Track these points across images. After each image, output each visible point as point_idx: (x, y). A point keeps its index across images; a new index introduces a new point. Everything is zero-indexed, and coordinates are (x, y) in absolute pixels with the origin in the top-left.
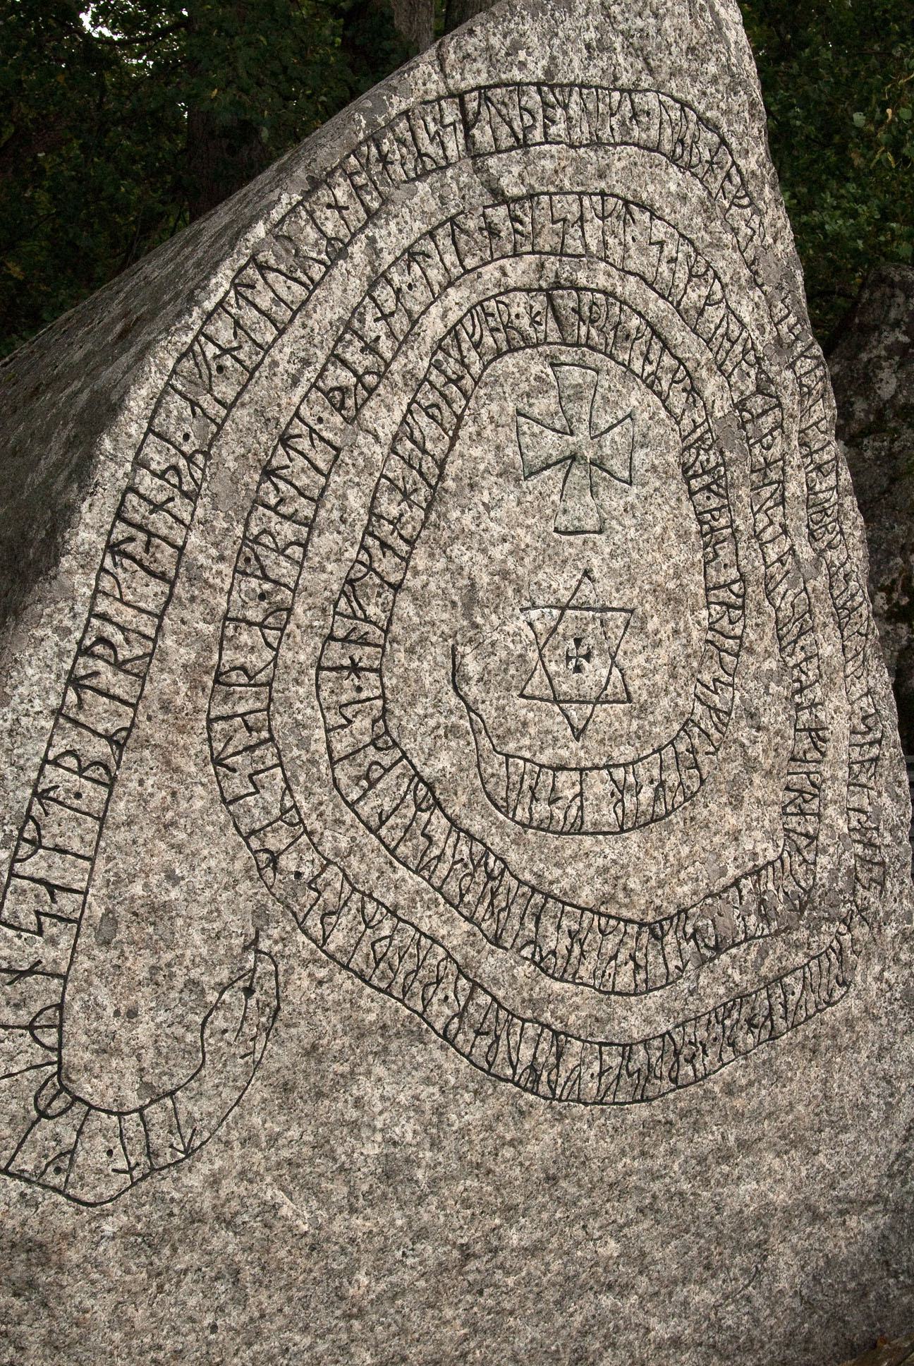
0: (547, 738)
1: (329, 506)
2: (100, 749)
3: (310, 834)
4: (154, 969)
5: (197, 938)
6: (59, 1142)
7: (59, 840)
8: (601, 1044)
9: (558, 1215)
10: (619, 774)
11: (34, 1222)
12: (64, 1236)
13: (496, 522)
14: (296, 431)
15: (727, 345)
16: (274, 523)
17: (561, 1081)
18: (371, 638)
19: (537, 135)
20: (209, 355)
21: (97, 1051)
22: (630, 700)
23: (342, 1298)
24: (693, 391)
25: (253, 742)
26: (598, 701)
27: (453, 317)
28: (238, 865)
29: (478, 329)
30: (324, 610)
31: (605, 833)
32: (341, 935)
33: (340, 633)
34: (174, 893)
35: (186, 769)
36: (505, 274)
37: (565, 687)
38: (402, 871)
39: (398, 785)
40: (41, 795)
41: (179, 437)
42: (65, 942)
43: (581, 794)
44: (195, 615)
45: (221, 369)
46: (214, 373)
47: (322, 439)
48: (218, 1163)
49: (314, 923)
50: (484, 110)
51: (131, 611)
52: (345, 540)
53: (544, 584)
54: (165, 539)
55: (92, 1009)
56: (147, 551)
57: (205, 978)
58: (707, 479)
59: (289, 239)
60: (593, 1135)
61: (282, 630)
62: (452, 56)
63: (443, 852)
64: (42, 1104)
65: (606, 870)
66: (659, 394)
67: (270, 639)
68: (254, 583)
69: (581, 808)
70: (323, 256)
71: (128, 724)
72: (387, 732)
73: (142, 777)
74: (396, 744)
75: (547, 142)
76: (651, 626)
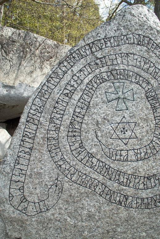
0: (118, 145)
1: (66, 111)
2: (28, 150)
3: (68, 162)
4: (39, 182)
5: (47, 178)
6: (25, 206)
7: (22, 163)
8: (136, 198)
9: (129, 227)
10: (136, 151)
11: (20, 217)
12: (25, 220)
13: (101, 110)
14: (59, 101)
15: (156, 74)
16: (56, 115)
17: (127, 204)
18: (77, 131)
19: (104, 47)
20: (43, 92)
21: (30, 193)
22: (137, 138)
23: (82, 235)
24: (148, 83)
25: (56, 148)
26: (129, 138)
27: (90, 79)
28: (54, 167)
29: (96, 80)
30: (67, 127)
31: (133, 161)
32: (74, 178)
33: (70, 131)
34: (42, 171)
35: (44, 152)
36: (101, 70)
37: (121, 137)
38: (87, 168)
39: (85, 154)
40: (18, 157)
41: (38, 104)
42: (24, 177)
43: (127, 154)
44: (42, 130)
45: (45, 94)
46: (44, 94)
47: (64, 101)
48: (53, 212)
49: (69, 176)
50: (93, 46)
51: (31, 130)
52: (69, 116)
53: (114, 120)
54: (36, 119)
55: (29, 188)
56: (33, 121)
57: (48, 184)
59: (56, 73)
60: (134, 212)
61: (59, 131)
62: (86, 39)
63: (96, 165)
64: (22, 200)
65: (133, 168)
66: (139, 85)
67: (57, 133)
68: (53, 124)
69: (127, 157)
70: (62, 74)
71: (32, 146)
72: (82, 146)
73: (35, 154)
74: (84, 148)
75: (106, 47)
76: (141, 125)
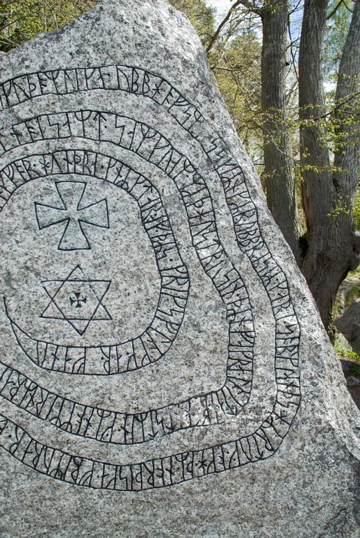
8: (104, 463)
22: (111, 319)
26: (91, 319)
58: (156, 223)
75: (43, 94)
